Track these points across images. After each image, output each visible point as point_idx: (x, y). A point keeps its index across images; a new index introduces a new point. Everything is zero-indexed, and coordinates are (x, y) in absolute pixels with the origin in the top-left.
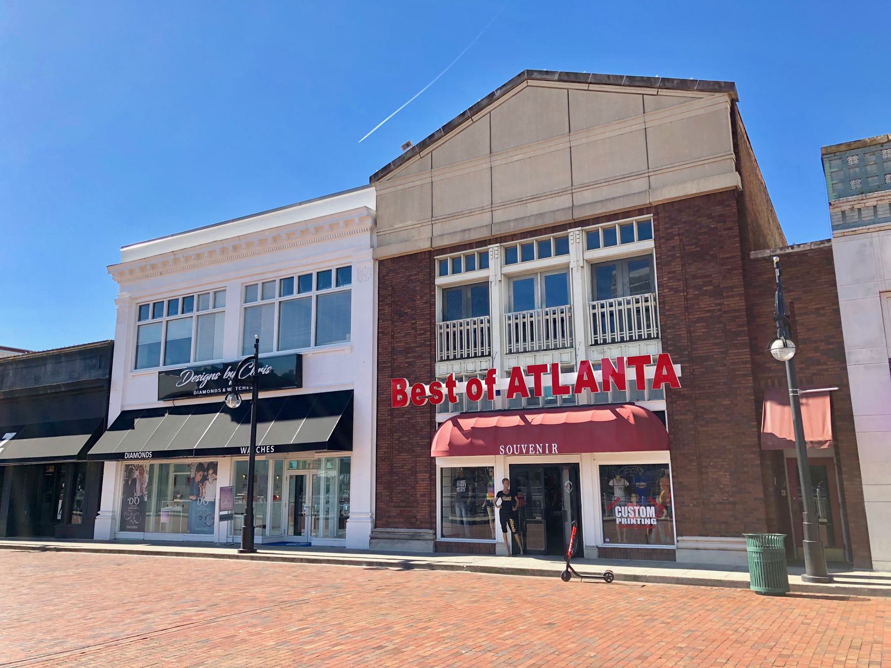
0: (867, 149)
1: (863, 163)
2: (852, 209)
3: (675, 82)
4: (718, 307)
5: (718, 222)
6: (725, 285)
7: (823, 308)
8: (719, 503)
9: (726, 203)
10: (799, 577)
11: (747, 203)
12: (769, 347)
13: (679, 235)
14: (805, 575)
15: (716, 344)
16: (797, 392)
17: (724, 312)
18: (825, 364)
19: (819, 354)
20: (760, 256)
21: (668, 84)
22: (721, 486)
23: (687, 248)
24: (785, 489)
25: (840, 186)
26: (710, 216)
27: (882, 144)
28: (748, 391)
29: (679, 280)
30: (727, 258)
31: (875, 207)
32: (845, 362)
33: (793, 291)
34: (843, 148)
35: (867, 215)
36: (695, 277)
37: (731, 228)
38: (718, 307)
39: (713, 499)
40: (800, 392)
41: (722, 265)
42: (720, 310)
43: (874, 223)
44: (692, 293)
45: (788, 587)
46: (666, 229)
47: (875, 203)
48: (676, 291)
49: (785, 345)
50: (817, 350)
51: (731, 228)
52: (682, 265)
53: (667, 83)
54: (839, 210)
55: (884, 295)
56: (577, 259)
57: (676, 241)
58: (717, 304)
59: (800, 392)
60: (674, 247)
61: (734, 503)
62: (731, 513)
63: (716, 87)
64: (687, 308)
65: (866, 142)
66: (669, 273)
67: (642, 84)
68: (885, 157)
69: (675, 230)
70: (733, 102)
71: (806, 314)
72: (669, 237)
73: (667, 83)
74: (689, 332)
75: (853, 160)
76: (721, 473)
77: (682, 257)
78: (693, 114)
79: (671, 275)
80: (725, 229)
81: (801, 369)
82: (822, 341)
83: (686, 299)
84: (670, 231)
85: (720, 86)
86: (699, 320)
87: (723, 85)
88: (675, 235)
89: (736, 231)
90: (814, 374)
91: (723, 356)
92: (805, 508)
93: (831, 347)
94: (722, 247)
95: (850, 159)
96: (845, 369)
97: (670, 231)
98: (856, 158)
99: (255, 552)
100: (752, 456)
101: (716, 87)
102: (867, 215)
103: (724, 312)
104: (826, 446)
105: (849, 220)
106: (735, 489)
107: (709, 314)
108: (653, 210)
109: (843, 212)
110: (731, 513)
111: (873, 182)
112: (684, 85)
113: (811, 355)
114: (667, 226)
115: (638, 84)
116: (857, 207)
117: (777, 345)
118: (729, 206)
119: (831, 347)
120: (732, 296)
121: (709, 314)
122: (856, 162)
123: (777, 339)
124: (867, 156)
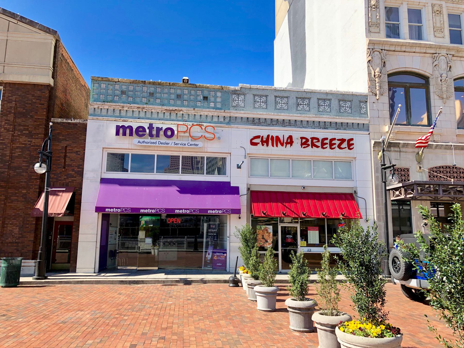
0: (110, 83)
1: (107, 89)
2: (98, 108)
3: (27, 20)
4: (29, 143)
5: (37, 100)
6: (35, 132)
7: (79, 151)
8: (10, 243)
9: (43, 91)
10: (32, 278)
11: (432, 108)
12: (34, 166)
13: (15, 101)
14: (35, 277)
15: (24, 161)
16: (48, 189)
17: (32, 146)
18: (75, 177)
19: (74, 173)
20: (56, 121)
21: (24, 20)
22: (13, 234)
23: (18, 109)
24: (52, 236)
25: (96, 96)
26: (33, 95)
27: (116, 82)
28: (36, 187)
29: (11, 125)
30: (39, 119)
31: (108, 109)
32: (83, 178)
33: (68, 141)
34: (100, 79)
35: (104, 112)
36: (20, 125)
37: (43, 104)
38: (29, 143)
39: (7, 241)
40: (50, 189)
41: (35, 121)
42: (30, 144)
43: (106, 116)
44: (17, 133)
45: (19, 283)
46: (9, 96)
47: (108, 108)
48: (8, 130)
49: (40, 166)
50: (73, 170)
51: (43, 104)
52: (14, 118)
53: (22, 19)
54: (93, 107)
55: (105, 150)
56: (444, 52)
57: (13, 104)
58: (29, 141)
59: (50, 189)
60: (11, 107)
61: (18, 243)
62: (15, 248)
63: (48, 31)
64: (12, 141)
65: (109, 79)
66: (6, 120)
67: (9, 15)
68: (116, 88)
69: (14, 98)
70: (57, 41)
71: (71, 153)
72: (10, 102)
73: (22, 19)
74: (11, 153)
75: (103, 86)
76: (15, 227)
77: (14, 113)
78: (34, 40)
79: (7, 122)
80: (40, 104)
81: (65, 178)
82: (76, 167)
83: (13, 136)
84: (11, 98)
85: (50, 31)
86: (18, 148)
87: (51, 30)
88: (14, 101)
89: (45, 106)
90: (69, 182)
91: (27, 168)
92: (41, 244)
93: (80, 170)
94: (36, 113)
95: (102, 85)
96: (82, 181)
97: (11, 98)
98: (104, 85)
99: (46, 278)
100: (32, 219)
101: (48, 31)
102: (104, 112)
103: (32, 146)
104: (60, 216)
105: (96, 113)
106: (20, 236)
107: (24, 146)
108: (3, 85)
109: (95, 108)
110: (15, 248)
111: (110, 98)
112: (31, 23)
113: (70, 173)
114: (10, 95)
115: (7, 14)
116: (100, 107)
117: (37, 165)
118: (44, 92)
119: (80, 170)
120: (37, 138)
121: (24, 146)
122: (104, 87)
123: (38, 162)
124: (109, 85)
